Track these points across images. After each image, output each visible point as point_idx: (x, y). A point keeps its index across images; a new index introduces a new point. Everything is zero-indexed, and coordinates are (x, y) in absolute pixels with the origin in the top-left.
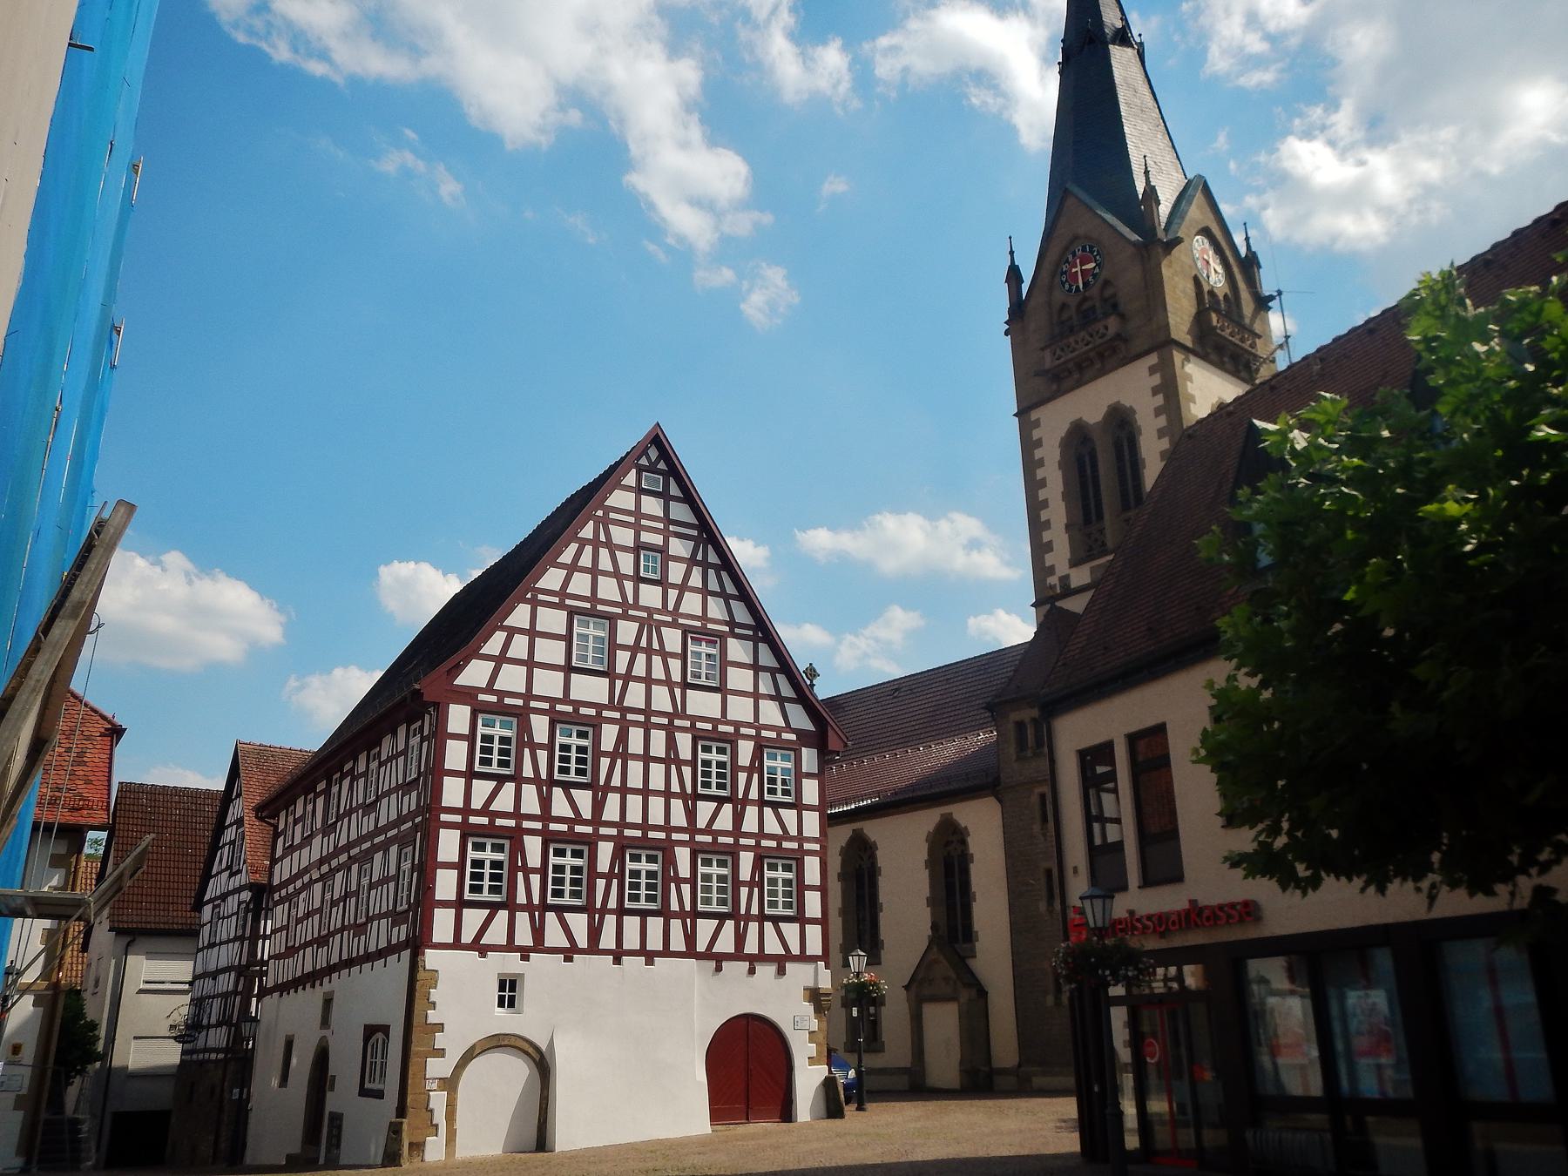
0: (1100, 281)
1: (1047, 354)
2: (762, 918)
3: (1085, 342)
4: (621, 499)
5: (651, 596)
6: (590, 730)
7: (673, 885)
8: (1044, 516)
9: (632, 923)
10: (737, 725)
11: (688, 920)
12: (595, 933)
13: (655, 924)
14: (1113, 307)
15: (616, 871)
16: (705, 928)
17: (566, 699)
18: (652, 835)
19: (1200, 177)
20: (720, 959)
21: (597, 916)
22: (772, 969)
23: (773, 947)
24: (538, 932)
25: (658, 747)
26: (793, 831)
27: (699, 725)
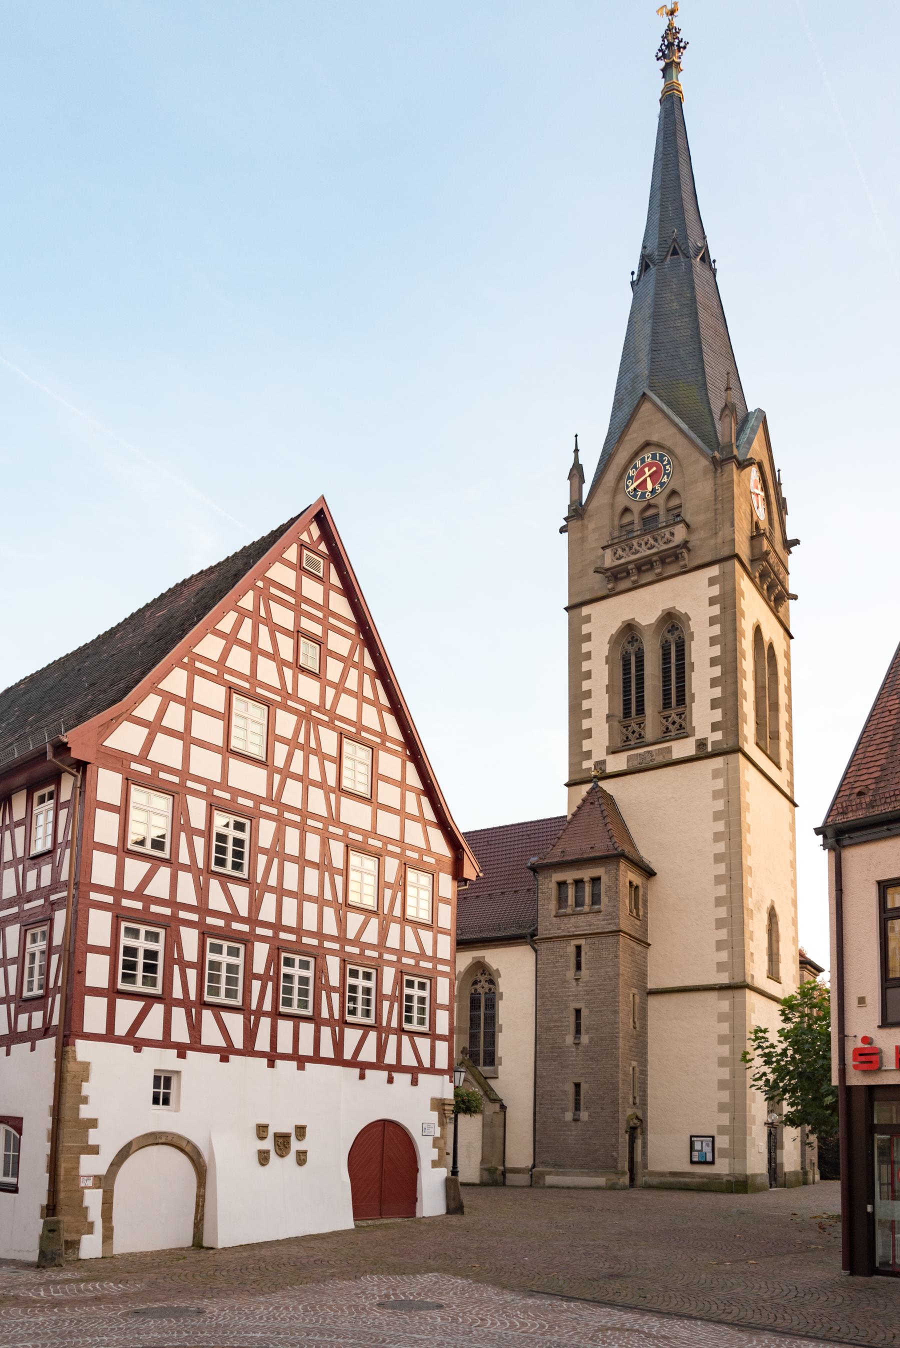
0: (667, 491)
1: (609, 552)
2: (401, 1031)
3: (649, 545)
4: (281, 574)
5: (309, 689)
6: (247, 823)
7: (324, 993)
8: (586, 705)
9: (285, 1027)
10: (388, 840)
11: (337, 1029)
12: (250, 1034)
13: (307, 1029)
14: (677, 516)
15: (271, 974)
16: (352, 1037)
17: (224, 785)
18: (305, 940)
19: (760, 410)
20: (363, 1067)
21: (252, 1017)
22: (408, 1077)
23: (409, 1059)
24: (195, 1028)
25: (313, 852)
26: (429, 953)
27: (351, 835)
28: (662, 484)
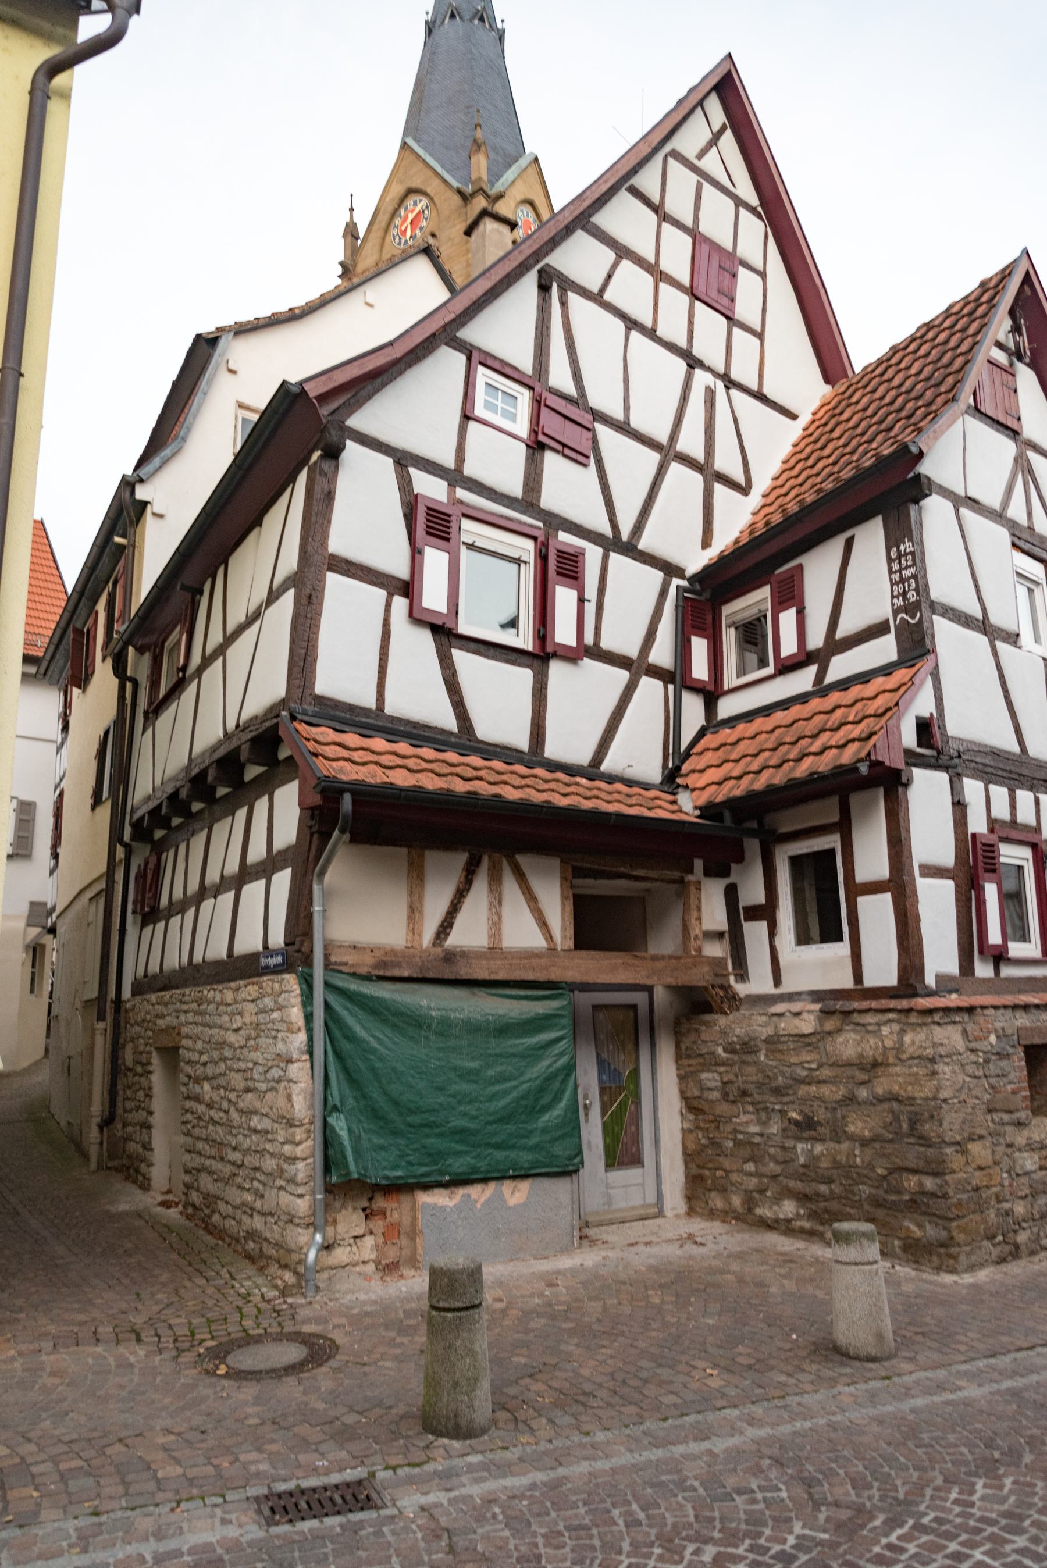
28: (421, 229)
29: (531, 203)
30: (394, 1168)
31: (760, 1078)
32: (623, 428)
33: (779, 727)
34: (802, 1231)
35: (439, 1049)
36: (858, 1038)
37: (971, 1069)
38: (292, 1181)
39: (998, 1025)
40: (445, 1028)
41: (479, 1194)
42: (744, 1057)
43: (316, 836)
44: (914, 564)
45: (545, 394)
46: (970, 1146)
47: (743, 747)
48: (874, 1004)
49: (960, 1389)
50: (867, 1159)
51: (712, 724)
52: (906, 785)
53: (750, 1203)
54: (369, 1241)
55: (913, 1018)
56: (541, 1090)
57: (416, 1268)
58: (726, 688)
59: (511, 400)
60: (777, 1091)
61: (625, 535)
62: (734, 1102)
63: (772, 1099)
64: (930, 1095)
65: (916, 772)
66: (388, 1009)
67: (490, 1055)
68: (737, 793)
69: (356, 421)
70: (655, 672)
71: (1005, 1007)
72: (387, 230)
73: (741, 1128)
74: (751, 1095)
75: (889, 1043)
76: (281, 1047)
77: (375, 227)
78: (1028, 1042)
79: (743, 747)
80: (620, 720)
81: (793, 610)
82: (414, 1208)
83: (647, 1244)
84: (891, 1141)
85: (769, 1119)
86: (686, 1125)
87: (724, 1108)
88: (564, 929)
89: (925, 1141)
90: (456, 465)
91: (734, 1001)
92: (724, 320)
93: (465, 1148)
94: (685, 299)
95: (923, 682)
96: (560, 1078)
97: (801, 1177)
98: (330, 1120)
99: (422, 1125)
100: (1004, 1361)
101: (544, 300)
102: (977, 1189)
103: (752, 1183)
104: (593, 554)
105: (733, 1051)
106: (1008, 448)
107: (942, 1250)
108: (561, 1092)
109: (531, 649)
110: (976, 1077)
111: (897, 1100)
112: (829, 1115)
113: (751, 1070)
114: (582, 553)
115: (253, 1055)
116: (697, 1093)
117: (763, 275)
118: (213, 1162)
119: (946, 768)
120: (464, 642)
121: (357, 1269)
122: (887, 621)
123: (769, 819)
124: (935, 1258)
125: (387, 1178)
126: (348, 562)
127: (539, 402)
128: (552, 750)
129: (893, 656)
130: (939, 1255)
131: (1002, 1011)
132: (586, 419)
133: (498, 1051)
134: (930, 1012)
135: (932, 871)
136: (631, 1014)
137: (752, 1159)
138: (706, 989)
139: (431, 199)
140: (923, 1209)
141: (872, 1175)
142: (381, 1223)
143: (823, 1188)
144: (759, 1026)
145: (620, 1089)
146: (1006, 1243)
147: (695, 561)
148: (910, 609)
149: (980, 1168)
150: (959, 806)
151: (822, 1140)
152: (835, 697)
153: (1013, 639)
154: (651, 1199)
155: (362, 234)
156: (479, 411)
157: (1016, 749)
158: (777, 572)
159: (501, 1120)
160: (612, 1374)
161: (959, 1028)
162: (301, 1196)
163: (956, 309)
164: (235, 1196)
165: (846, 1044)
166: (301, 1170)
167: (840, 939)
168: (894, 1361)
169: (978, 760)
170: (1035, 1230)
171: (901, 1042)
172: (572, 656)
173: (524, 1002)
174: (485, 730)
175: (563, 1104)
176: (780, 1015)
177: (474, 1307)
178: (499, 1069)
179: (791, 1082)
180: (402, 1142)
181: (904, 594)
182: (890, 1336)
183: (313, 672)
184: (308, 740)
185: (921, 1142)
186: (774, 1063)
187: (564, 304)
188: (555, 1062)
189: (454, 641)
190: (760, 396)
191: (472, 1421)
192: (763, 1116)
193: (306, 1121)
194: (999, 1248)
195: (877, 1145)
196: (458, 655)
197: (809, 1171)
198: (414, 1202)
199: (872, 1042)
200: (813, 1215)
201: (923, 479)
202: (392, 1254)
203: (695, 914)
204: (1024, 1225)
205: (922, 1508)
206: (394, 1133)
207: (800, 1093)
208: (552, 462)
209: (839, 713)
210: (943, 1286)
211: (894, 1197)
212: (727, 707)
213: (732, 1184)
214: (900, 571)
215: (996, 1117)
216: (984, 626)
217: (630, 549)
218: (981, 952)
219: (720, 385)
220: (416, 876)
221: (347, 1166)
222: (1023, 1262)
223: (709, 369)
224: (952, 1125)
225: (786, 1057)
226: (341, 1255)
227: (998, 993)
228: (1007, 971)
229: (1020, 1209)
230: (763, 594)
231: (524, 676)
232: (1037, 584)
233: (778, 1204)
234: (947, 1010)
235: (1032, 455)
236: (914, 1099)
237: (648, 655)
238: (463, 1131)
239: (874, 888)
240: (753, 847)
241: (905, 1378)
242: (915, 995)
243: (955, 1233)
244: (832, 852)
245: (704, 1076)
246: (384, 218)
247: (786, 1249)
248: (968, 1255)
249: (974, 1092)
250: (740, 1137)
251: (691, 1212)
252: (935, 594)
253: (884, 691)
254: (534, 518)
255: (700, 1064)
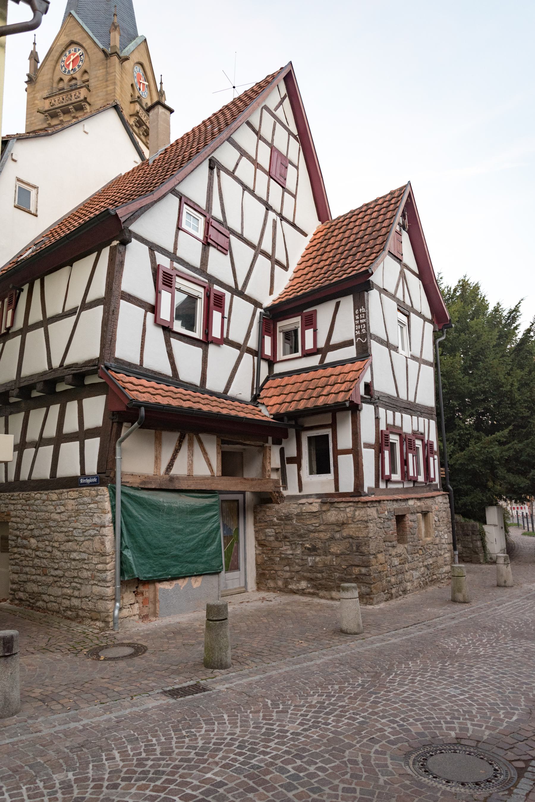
28: (79, 66)
29: (141, 64)
30: (149, 573)
31: (293, 530)
32: (240, 237)
33: (306, 381)
34: (309, 593)
35: (167, 520)
36: (337, 513)
37: (379, 525)
38: (104, 581)
39: (388, 507)
40: (170, 511)
41: (182, 583)
42: (286, 522)
43: (115, 424)
44: (365, 318)
45: (211, 220)
46: (378, 555)
47: (288, 389)
48: (344, 499)
49: (390, 640)
50: (338, 562)
51: (271, 376)
52: (360, 411)
53: (286, 583)
54: (136, 606)
55: (360, 505)
56: (208, 537)
57: (156, 617)
58: (278, 360)
59: (196, 221)
60: (300, 536)
61: (240, 288)
62: (280, 541)
63: (298, 539)
64: (365, 535)
65: (364, 405)
66: (147, 503)
67: (187, 523)
68: (291, 409)
69: (134, 227)
70: (250, 351)
71: (391, 500)
72: (57, 62)
73: (284, 552)
74: (289, 538)
75: (349, 515)
76: (96, 520)
77: (50, 58)
78: (397, 514)
79: (288, 389)
80: (236, 373)
81: (312, 330)
82: (155, 590)
83: (248, 602)
84: (348, 554)
85: (296, 548)
86: (258, 552)
87: (276, 544)
88: (218, 467)
89: (362, 554)
90: (174, 251)
91: (282, 498)
92: (281, 188)
93: (178, 564)
94: (267, 177)
95: (367, 368)
96: (215, 532)
97: (310, 571)
98: (125, 552)
99: (160, 554)
100: (401, 631)
101: (211, 174)
102: (380, 572)
103: (288, 575)
104: (228, 295)
105: (281, 520)
106: (397, 267)
107: (368, 596)
108: (215, 538)
109: (201, 339)
110: (381, 528)
111: (352, 538)
112: (323, 545)
113: (289, 527)
114: (224, 295)
115: (73, 524)
116: (263, 538)
117: (297, 168)
118: (38, 577)
119: (373, 403)
120: (176, 335)
121: (132, 618)
122: (353, 340)
123: (301, 420)
124: (365, 600)
125: (145, 577)
126: (129, 295)
127: (208, 223)
128: (209, 386)
129: (354, 355)
130: (366, 598)
131: (389, 502)
132: (226, 232)
133: (191, 521)
134: (366, 502)
135: (368, 446)
136: (236, 504)
137: (288, 565)
138: (271, 493)
139: (85, 50)
140: (361, 581)
141: (340, 568)
142: (141, 597)
143: (319, 575)
144: (293, 509)
145: (231, 537)
146: (389, 593)
147: (267, 301)
148: (363, 336)
149: (381, 564)
150: (377, 419)
151: (320, 556)
152: (330, 371)
153: (396, 349)
154: (243, 584)
155: (41, 58)
156: (184, 226)
157: (396, 395)
158: (304, 311)
159: (192, 551)
160: (265, 645)
161: (375, 508)
162: (108, 587)
163: (380, 202)
164: (55, 591)
165: (331, 516)
166: (109, 575)
167: (328, 472)
168: (363, 634)
169: (384, 400)
170: (397, 588)
171: (354, 515)
172: (218, 342)
173: (201, 499)
174: (184, 376)
175: (216, 543)
176: (303, 504)
177: (226, 619)
178: (191, 528)
179: (307, 532)
180: (151, 561)
181: (360, 330)
182: (361, 625)
183: (114, 346)
184: (118, 380)
185: (361, 554)
186: (299, 524)
187: (219, 176)
188: (213, 525)
189: (172, 334)
190: (293, 225)
191: (226, 662)
192: (294, 546)
193: (111, 553)
194: (386, 595)
195: (343, 556)
196: (173, 341)
197: (313, 568)
198: (155, 587)
199: (342, 515)
200: (314, 587)
201: (371, 283)
202: (146, 611)
203: (268, 460)
204: (394, 586)
205: (395, 670)
206: (148, 558)
207: (311, 536)
208: (213, 252)
209: (333, 378)
210: (369, 610)
211: (349, 577)
212: (278, 368)
213: (278, 576)
214: (359, 319)
215: (387, 543)
216: (387, 344)
217: (241, 294)
218: (382, 478)
219: (278, 219)
220: (158, 442)
221: (133, 572)
222: (394, 600)
223: (274, 211)
224: (373, 547)
225: (304, 522)
226: (125, 612)
227: (387, 495)
228: (390, 486)
229: (393, 580)
230: (298, 319)
231: (198, 351)
232: (405, 325)
233: (299, 583)
234: (372, 502)
235: (406, 271)
236: (359, 537)
237: (247, 343)
238: (177, 556)
239: (345, 452)
240: (292, 432)
241: (370, 639)
242: (361, 496)
243: (372, 589)
244: (327, 436)
245: (267, 530)
246: (56, 54)
247: (304, 600)
248: (377, 598)
249: (380, 534)
250: (283, 556)
251: (259, 589)
252: (372, 331)
253: (352, 371)
254: (204, 278)
255: (266, 525)
